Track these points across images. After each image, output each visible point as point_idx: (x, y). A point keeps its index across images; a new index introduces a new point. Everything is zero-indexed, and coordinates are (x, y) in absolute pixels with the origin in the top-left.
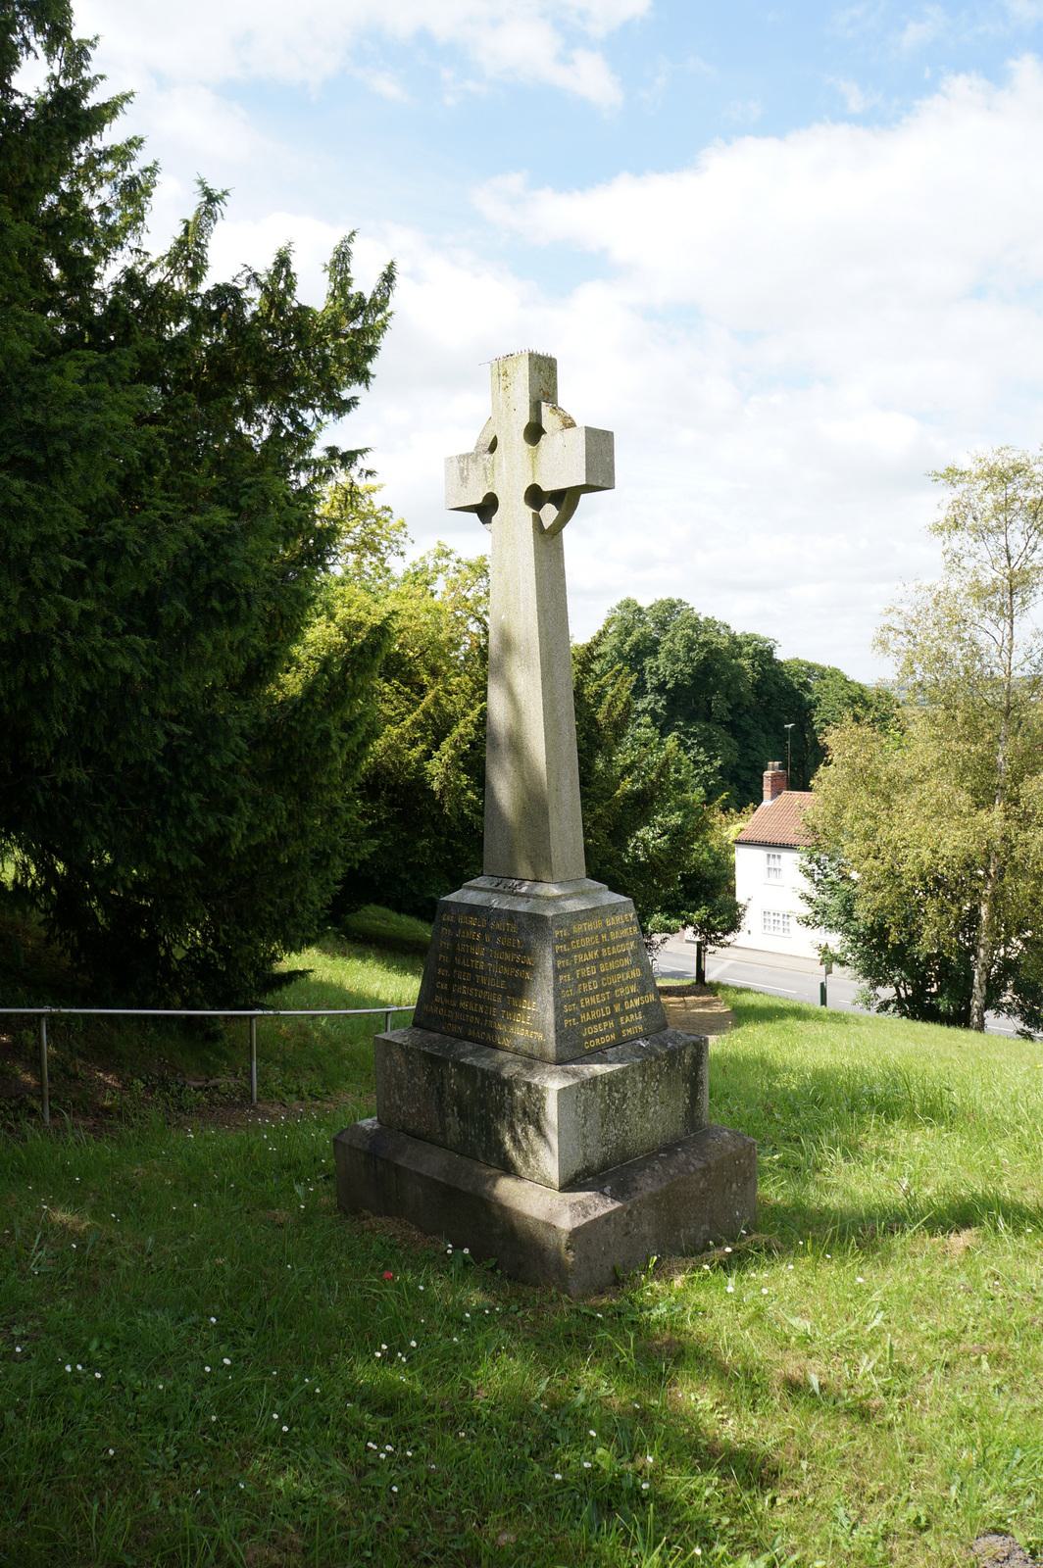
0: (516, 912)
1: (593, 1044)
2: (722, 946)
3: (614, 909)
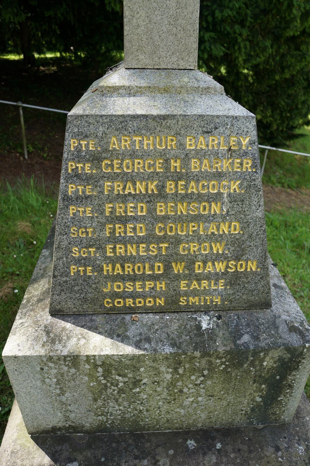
1: (119, 303)
3: (209, 125)
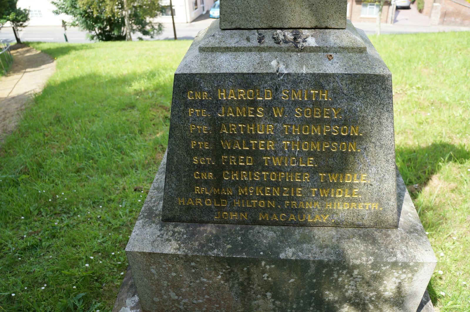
0: (326, 76)
2: (24, 27)
